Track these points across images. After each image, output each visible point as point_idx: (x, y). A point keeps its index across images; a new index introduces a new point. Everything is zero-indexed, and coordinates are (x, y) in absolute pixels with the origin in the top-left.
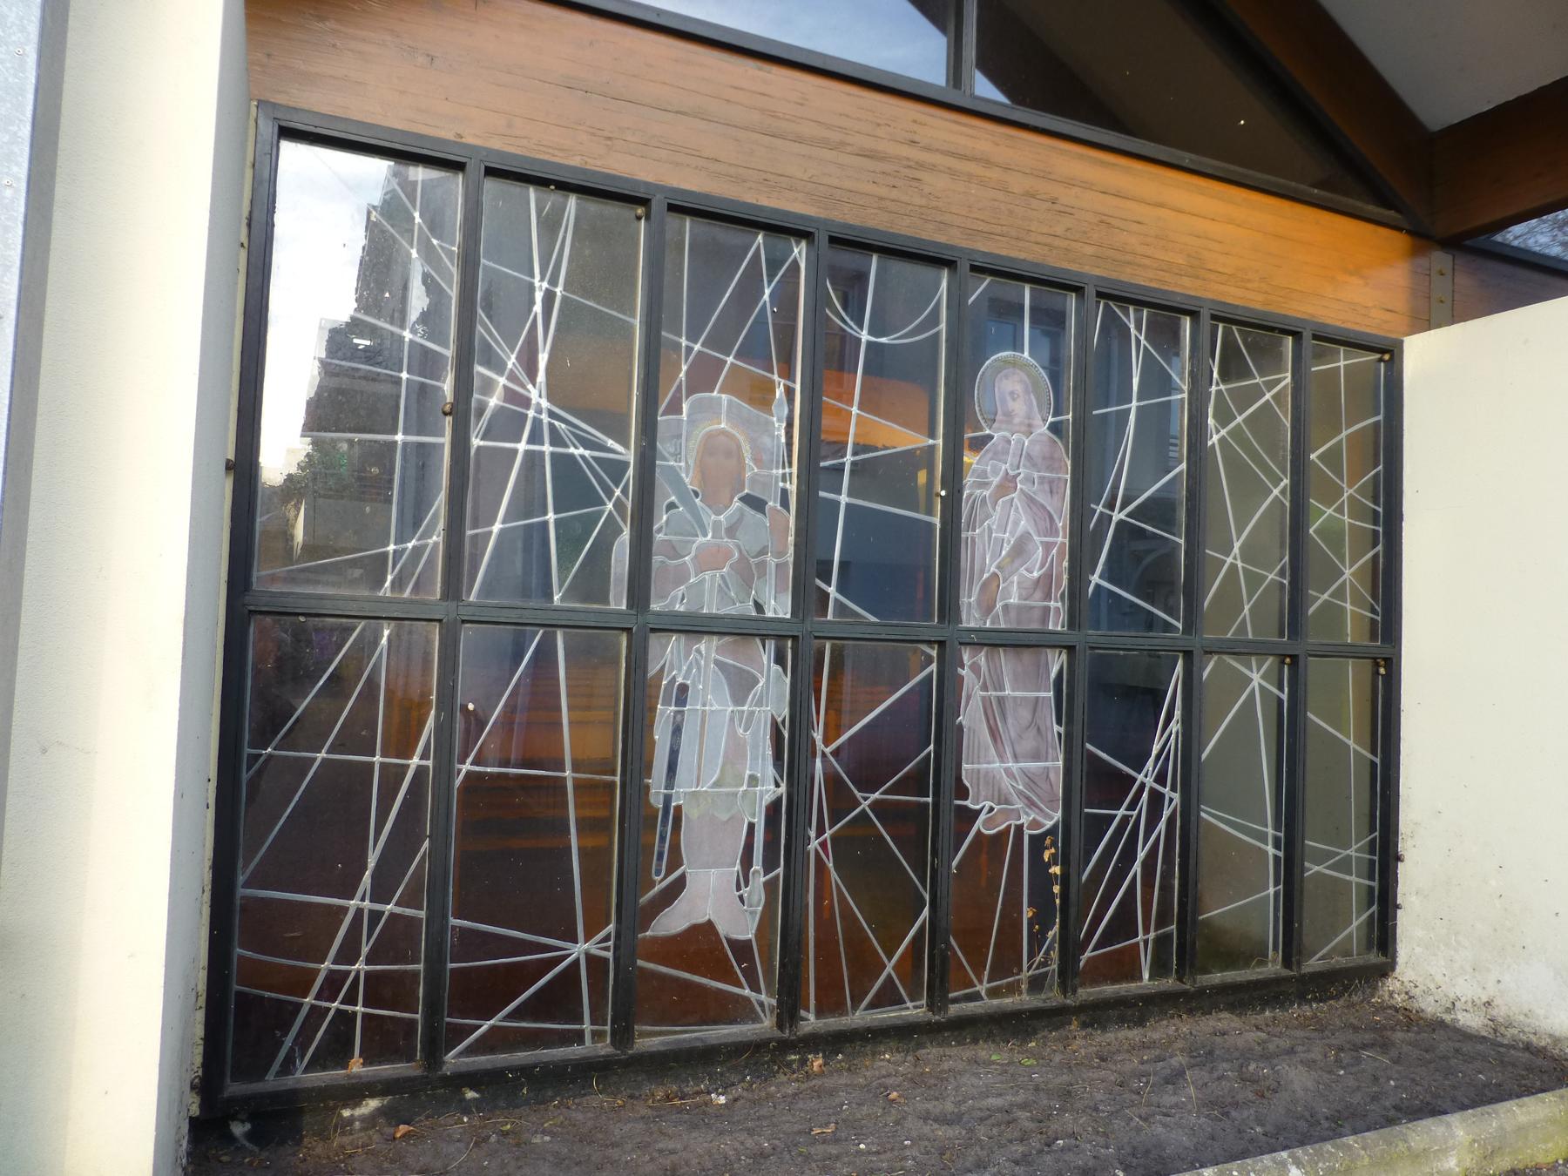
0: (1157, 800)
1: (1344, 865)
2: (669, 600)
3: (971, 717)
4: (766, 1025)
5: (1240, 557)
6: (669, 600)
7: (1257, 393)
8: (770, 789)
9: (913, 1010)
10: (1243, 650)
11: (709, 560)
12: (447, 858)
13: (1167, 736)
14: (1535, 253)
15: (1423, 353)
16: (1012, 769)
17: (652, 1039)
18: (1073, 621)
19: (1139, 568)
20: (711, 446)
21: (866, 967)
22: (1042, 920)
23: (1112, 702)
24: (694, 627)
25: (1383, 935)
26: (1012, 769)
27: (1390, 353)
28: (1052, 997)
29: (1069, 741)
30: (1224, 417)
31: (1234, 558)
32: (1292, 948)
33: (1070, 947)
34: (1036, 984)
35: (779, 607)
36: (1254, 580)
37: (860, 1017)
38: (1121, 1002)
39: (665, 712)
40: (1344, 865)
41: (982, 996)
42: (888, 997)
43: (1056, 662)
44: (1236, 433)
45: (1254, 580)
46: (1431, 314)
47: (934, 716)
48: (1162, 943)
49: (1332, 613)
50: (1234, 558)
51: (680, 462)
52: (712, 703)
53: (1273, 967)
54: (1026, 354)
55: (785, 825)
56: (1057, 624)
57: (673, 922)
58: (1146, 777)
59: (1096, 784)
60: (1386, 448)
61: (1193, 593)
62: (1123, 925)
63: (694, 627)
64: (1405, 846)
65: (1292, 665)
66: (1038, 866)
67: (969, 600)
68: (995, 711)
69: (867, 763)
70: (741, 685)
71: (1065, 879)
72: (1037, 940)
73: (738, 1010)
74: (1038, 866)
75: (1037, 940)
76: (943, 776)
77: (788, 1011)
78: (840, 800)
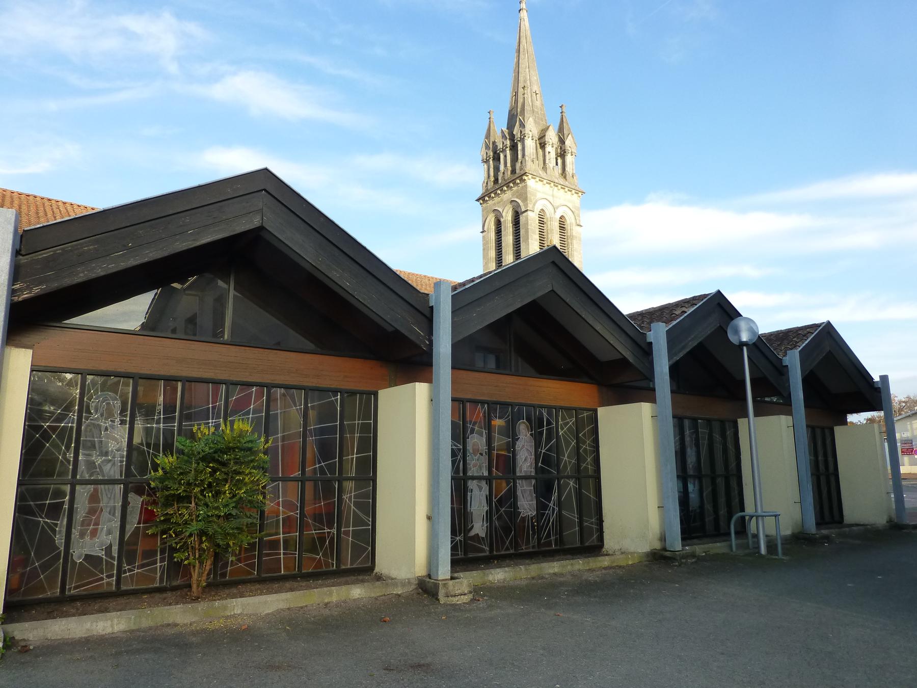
0: (553, 509)
1: (592, 523)
2: (470, 474)
3: (519, 493)
4: (488, 553)
5: (567, 458)
6: (470, 474)
7: (568, 423)
8: (486, 508)
9: (512, 551)
10: (569, 477)
11: (475, 466)
12: (295, 625)
13: (555, 497)
14: (353, 583)
15: (602, 411)
16: (527, 505)
17: (471, 555)
18: (536, 473)
19: (546, 463)
20: (474, 445)
21: (504, 543)
22: (534, 534)
23: (544, 489)
24: (473, 478)
25: (601, 538)
26: (527, 505)
27: (596, 411)
28: (536, 550)
29: (537, 497)
30: (562, 429)
31: (566, 458)
32: (582, 542)
33: (539, 539)
34: (533, 547)
35: (486, 474)
36: (570, 462)
37: (503, 553)
38: (549, 551)
39: (469, 494)
40: (592, 523)
41: (524, 549)
42: (507, 549)
43: (533, 482)
44: (284, 554)
45: (570, 462)
46: (604, 404)
47: (512, 495)
48: (556, 540)
49: (586, 468)
50: (566, 458)
51: (470, 448)
52: (476, 492)
53: (578, 545)
54: (780, 556)
55: (489, 514)
56: (533, 474)
57: (472, 533)
58: (551, 505)
59: (542, 507)
60: (595, 431)
61: (558, 465)
62: (549, 535)
63: (473, 478)
64: (604, 518)
65: (578, 480)
66: (532, 523)
67: (518, 470)
68: (523, 492)
69: (500, 502)
70: (480, 488)
71: (538, 526)
72: (533, 538)
73: (483, 551)
74: (532, 523)
75: (533, 538)
76: (515, 505)
77: (491, 550)
78: (498, 511)
